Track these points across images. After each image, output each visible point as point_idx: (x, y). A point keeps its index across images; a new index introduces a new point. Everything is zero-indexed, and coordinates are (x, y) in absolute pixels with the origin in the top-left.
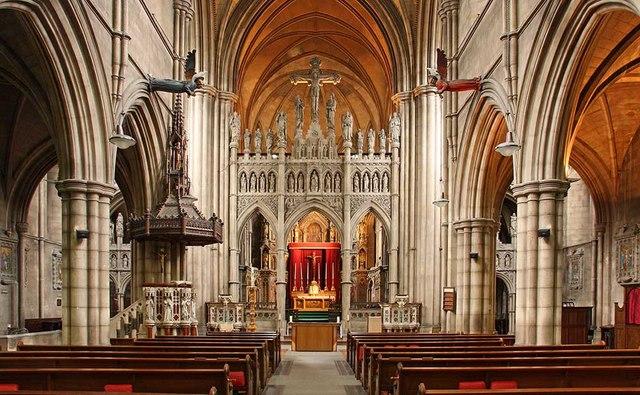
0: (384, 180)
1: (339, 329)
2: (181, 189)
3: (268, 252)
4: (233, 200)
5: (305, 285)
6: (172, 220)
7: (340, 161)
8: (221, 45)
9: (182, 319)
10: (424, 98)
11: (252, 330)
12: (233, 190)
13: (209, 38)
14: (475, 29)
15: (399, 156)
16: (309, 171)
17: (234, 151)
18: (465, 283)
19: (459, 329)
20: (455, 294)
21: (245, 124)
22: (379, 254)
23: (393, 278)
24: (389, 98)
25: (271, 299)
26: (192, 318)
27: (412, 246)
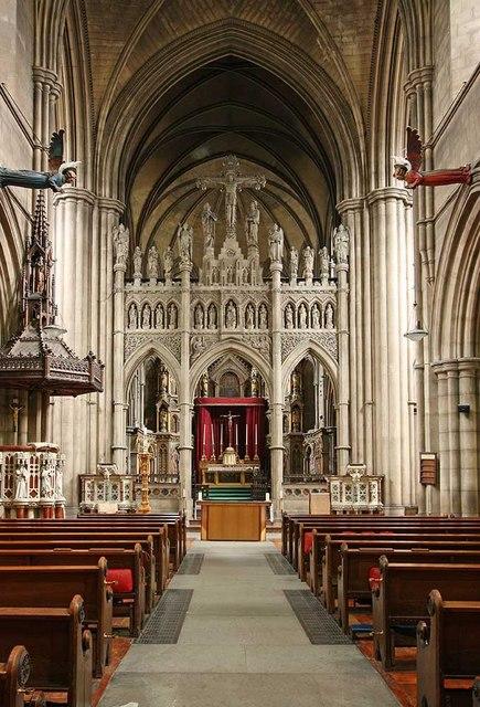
0: (327, 313)
1: (268, 511)
2: (44, 319)
3: (166, 410)
4: (119, 338)
5: (217, 453)
6: (30, 359)
7: (266, 288)
8: (100, 137)
9: (42, 496)
10: (382, 205)
11: (145, 511)
12: (119, 325)
13: (84, 129)
14: (459, 103)
15: (348, 281)
16: (224, 302)
17: (120, 276)
18: (452, 445)
19: (445, 511)
20: (437, 462)
21: (134, 241)
22: (320, 410)
23: (343, 441)
24: (334, 207)
25: (172, 469)
26: (57, 491)
27: (369, 399)
